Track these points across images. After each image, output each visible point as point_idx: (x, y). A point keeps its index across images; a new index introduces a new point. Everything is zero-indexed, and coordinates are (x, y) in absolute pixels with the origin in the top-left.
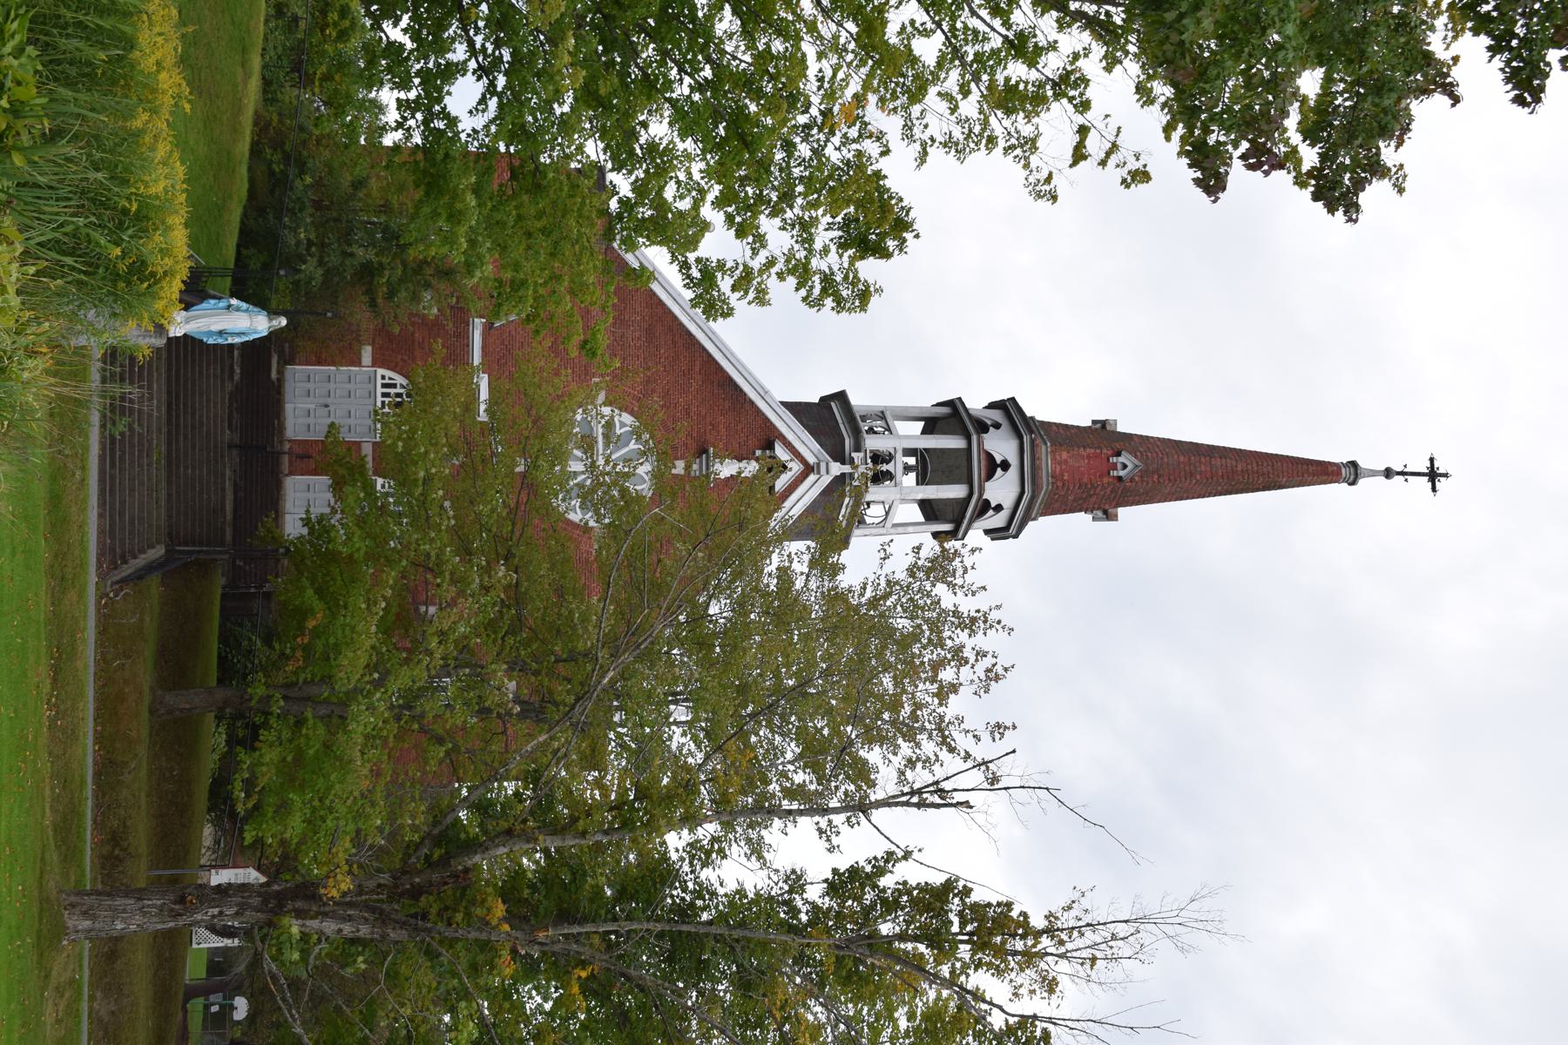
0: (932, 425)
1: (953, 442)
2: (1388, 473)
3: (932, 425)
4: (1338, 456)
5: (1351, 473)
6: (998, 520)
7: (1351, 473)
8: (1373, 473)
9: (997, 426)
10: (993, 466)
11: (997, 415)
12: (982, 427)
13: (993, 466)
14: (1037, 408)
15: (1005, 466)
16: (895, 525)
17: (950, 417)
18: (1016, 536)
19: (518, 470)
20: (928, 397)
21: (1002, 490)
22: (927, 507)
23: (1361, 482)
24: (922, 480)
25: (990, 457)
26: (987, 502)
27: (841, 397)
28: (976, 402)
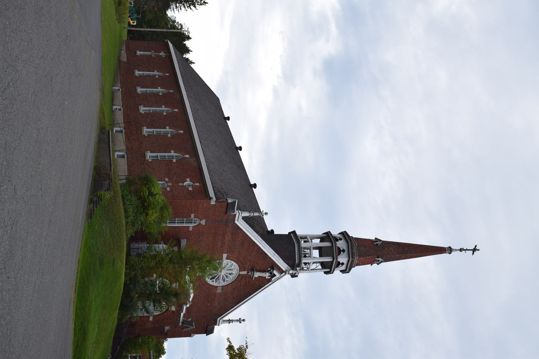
0: (322, 239)
1: (327, 244)
2: (461, 250)
3: (322, 239)
4: (445, 245)
5: (450, 250)
6: (343, 268)
7: (450, 250)
8: (456, 250)
9: (341, 239)
10: (340, 251)
11: (340, 236)
12: (336, 239)
13: (340, 251)
14: (353, 234)
15: (344, 251)
16: (312, 270)
17: (327, 237)
18: (348, 272)
19: (218, 291)
20: (320, 232)
21: (343, 259)
22: (322, 264)
23: (453, 253)
24: (321, 255)
25: (339, 248)
26: (339, 262)
27: (294, 232)
28: (335, 232)
